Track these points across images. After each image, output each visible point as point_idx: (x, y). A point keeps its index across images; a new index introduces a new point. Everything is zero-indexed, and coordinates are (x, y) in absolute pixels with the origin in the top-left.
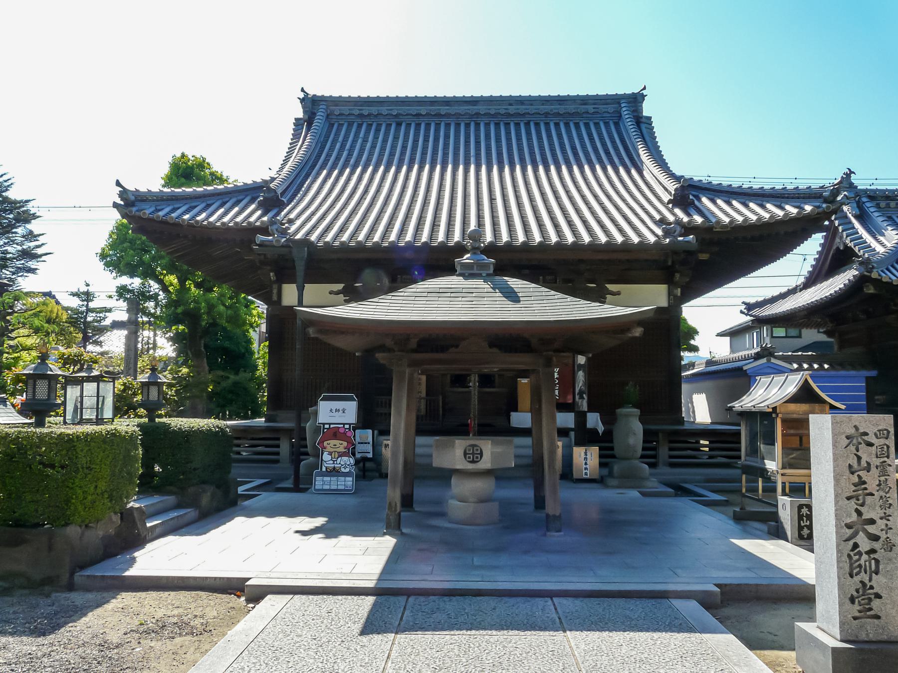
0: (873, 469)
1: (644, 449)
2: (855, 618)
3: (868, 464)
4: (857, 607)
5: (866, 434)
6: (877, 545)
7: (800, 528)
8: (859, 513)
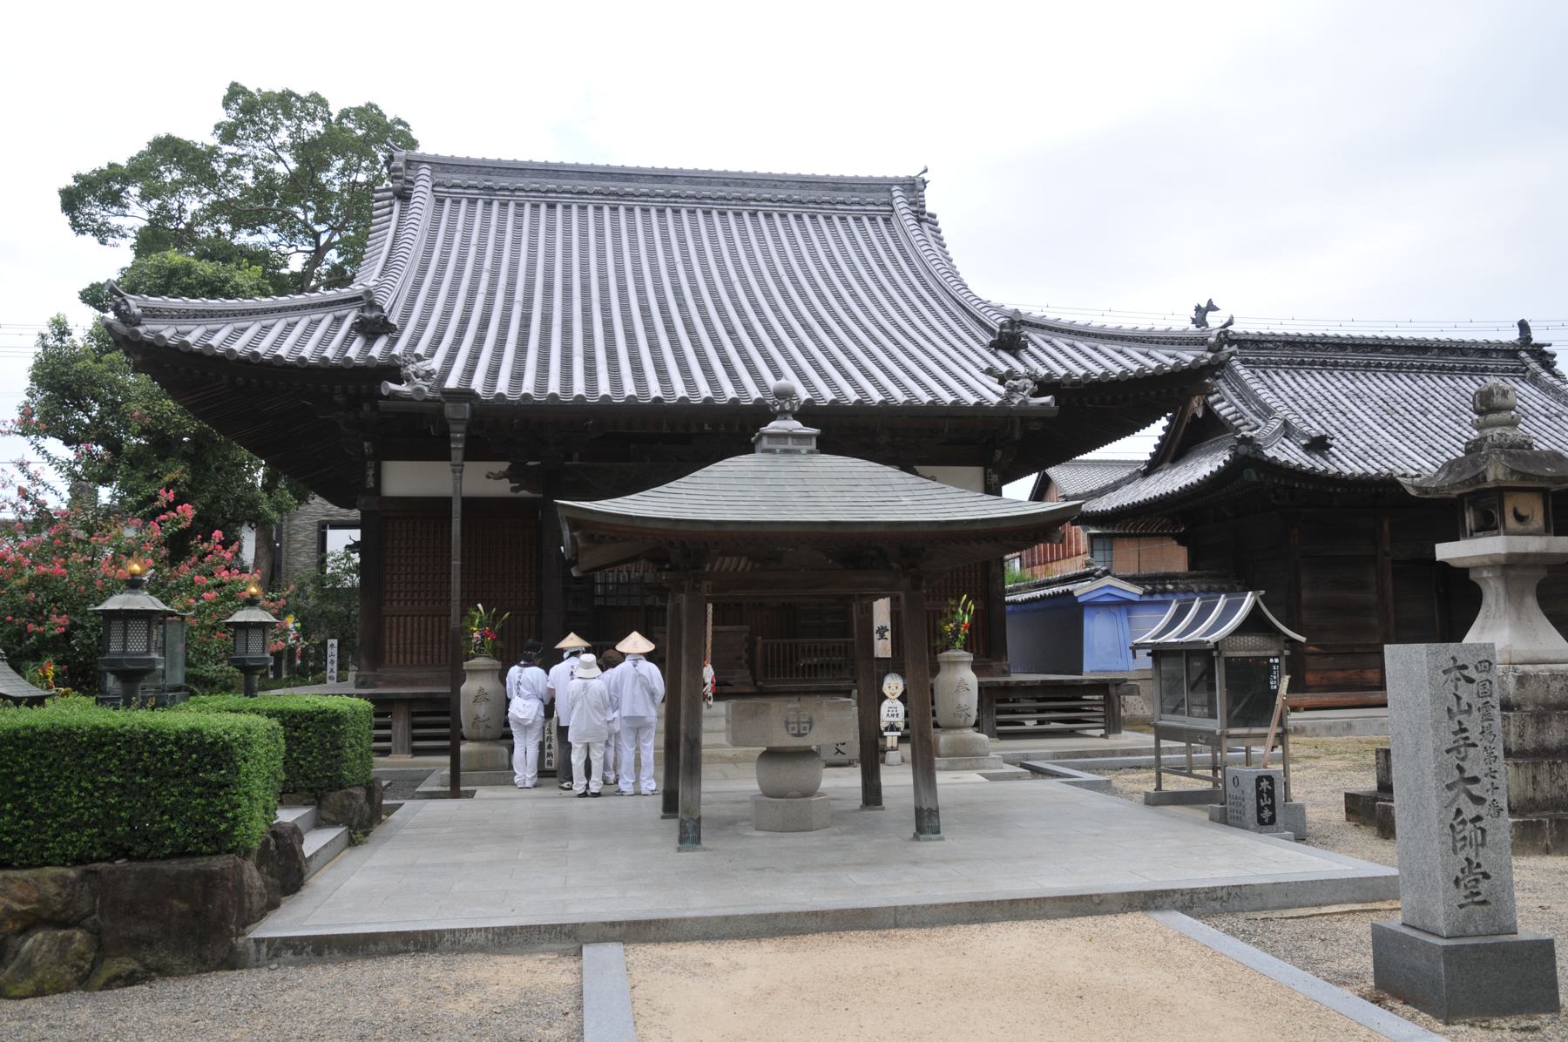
0: (1475, 713)
2: (1461, 906)
3: (1469, 706)
6: (1482, 810)
7: (1260, 810)
8: (1460, 769)
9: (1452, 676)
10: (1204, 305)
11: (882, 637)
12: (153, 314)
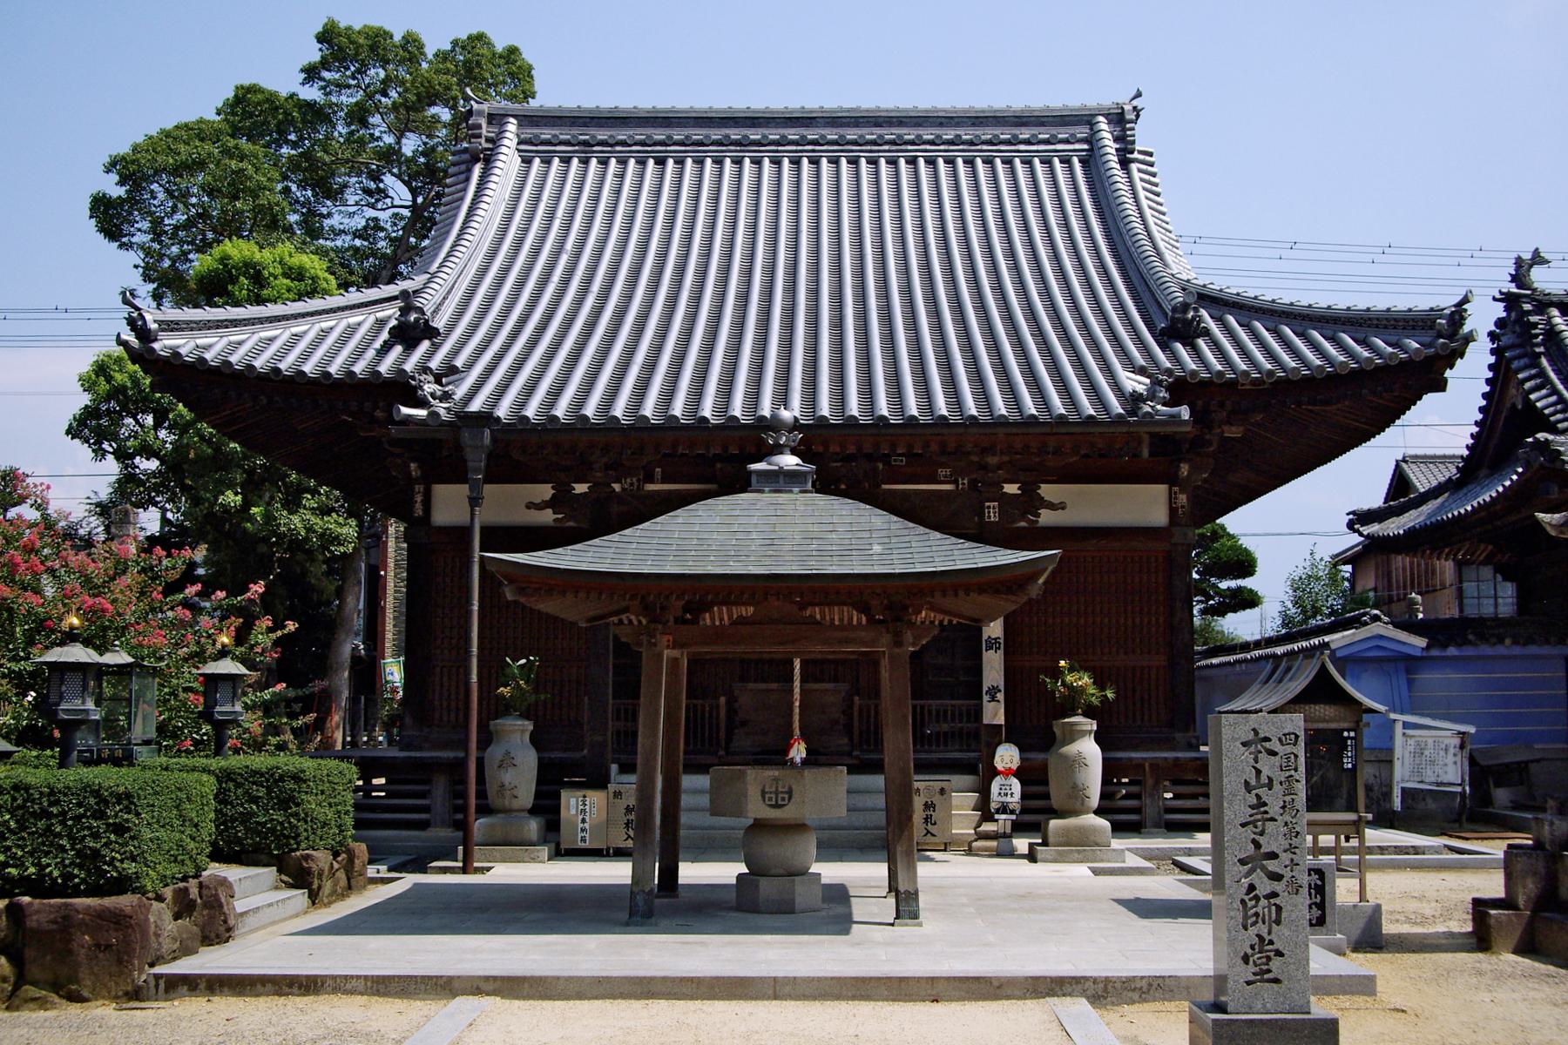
0: (1277, 786)
2: (1249, 983)
4: (1251, 968)
5: (1267, 739)
6: (1278, 887)
8: (1257, 845)
9: (1252, 749)
10: (1527, 256)
11: (993, 699)
12: (171, 326)
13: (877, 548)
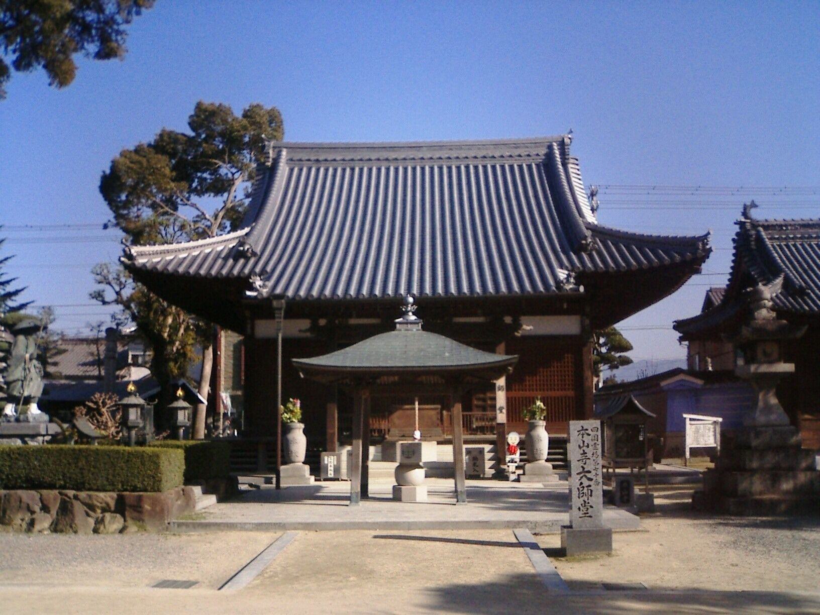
1: (549, 454)
6: (591, 483)
10: (748, 204)
11: (501, 412)
13: (447, 354)
